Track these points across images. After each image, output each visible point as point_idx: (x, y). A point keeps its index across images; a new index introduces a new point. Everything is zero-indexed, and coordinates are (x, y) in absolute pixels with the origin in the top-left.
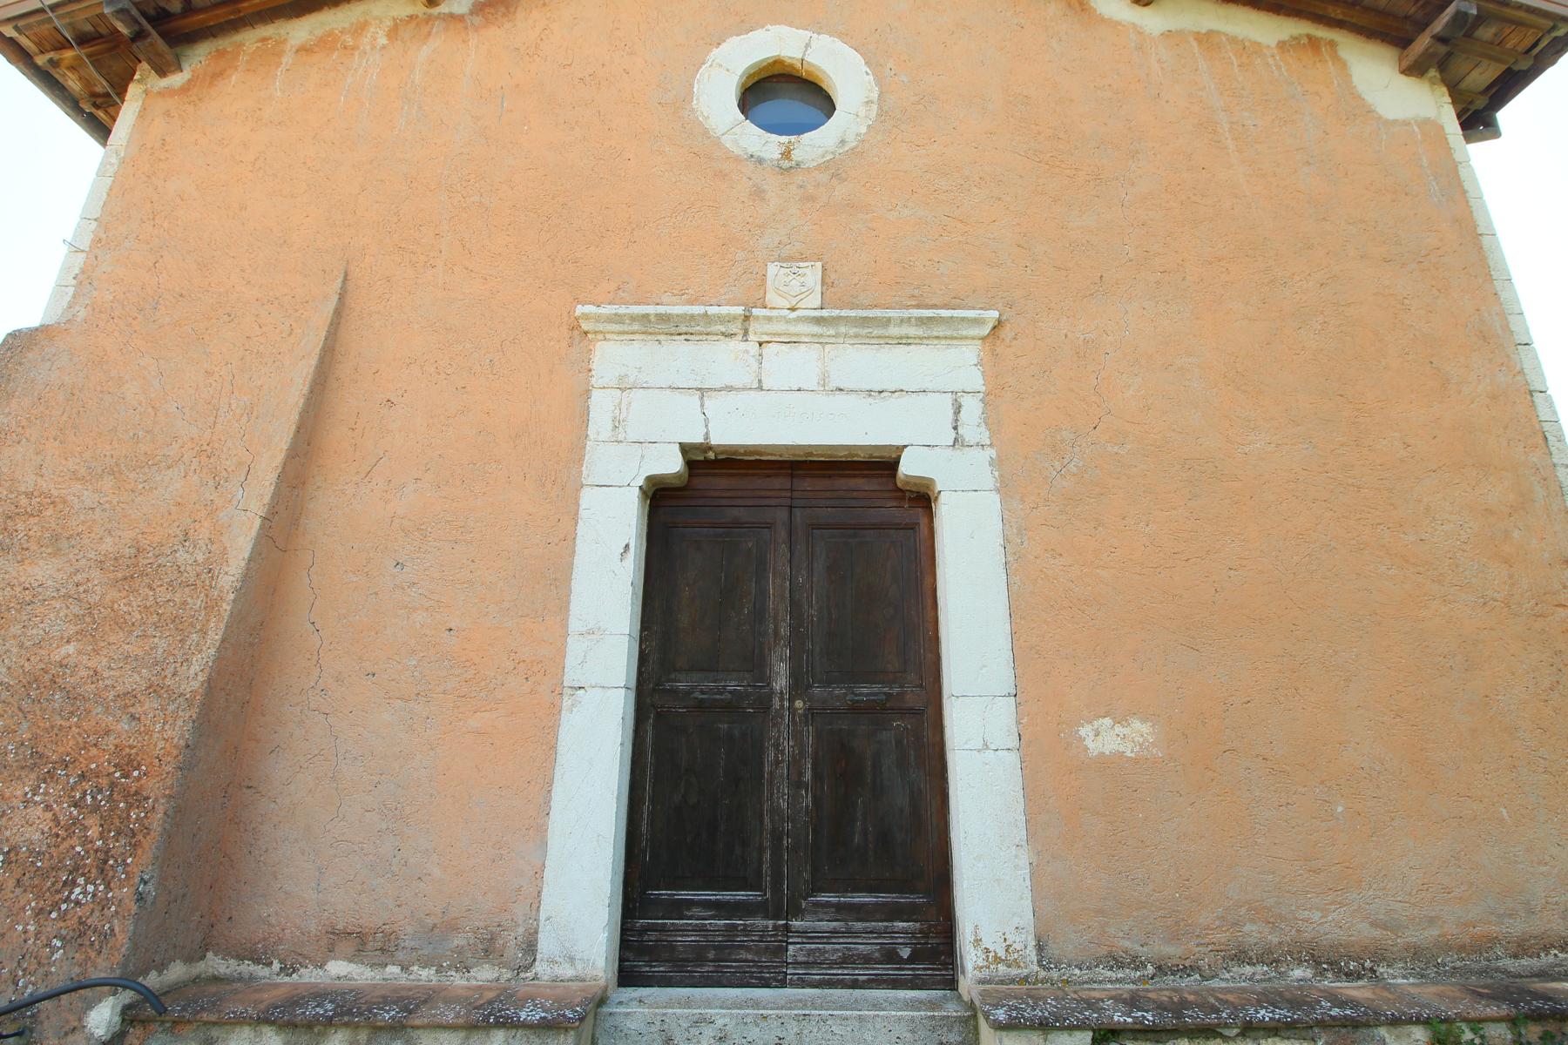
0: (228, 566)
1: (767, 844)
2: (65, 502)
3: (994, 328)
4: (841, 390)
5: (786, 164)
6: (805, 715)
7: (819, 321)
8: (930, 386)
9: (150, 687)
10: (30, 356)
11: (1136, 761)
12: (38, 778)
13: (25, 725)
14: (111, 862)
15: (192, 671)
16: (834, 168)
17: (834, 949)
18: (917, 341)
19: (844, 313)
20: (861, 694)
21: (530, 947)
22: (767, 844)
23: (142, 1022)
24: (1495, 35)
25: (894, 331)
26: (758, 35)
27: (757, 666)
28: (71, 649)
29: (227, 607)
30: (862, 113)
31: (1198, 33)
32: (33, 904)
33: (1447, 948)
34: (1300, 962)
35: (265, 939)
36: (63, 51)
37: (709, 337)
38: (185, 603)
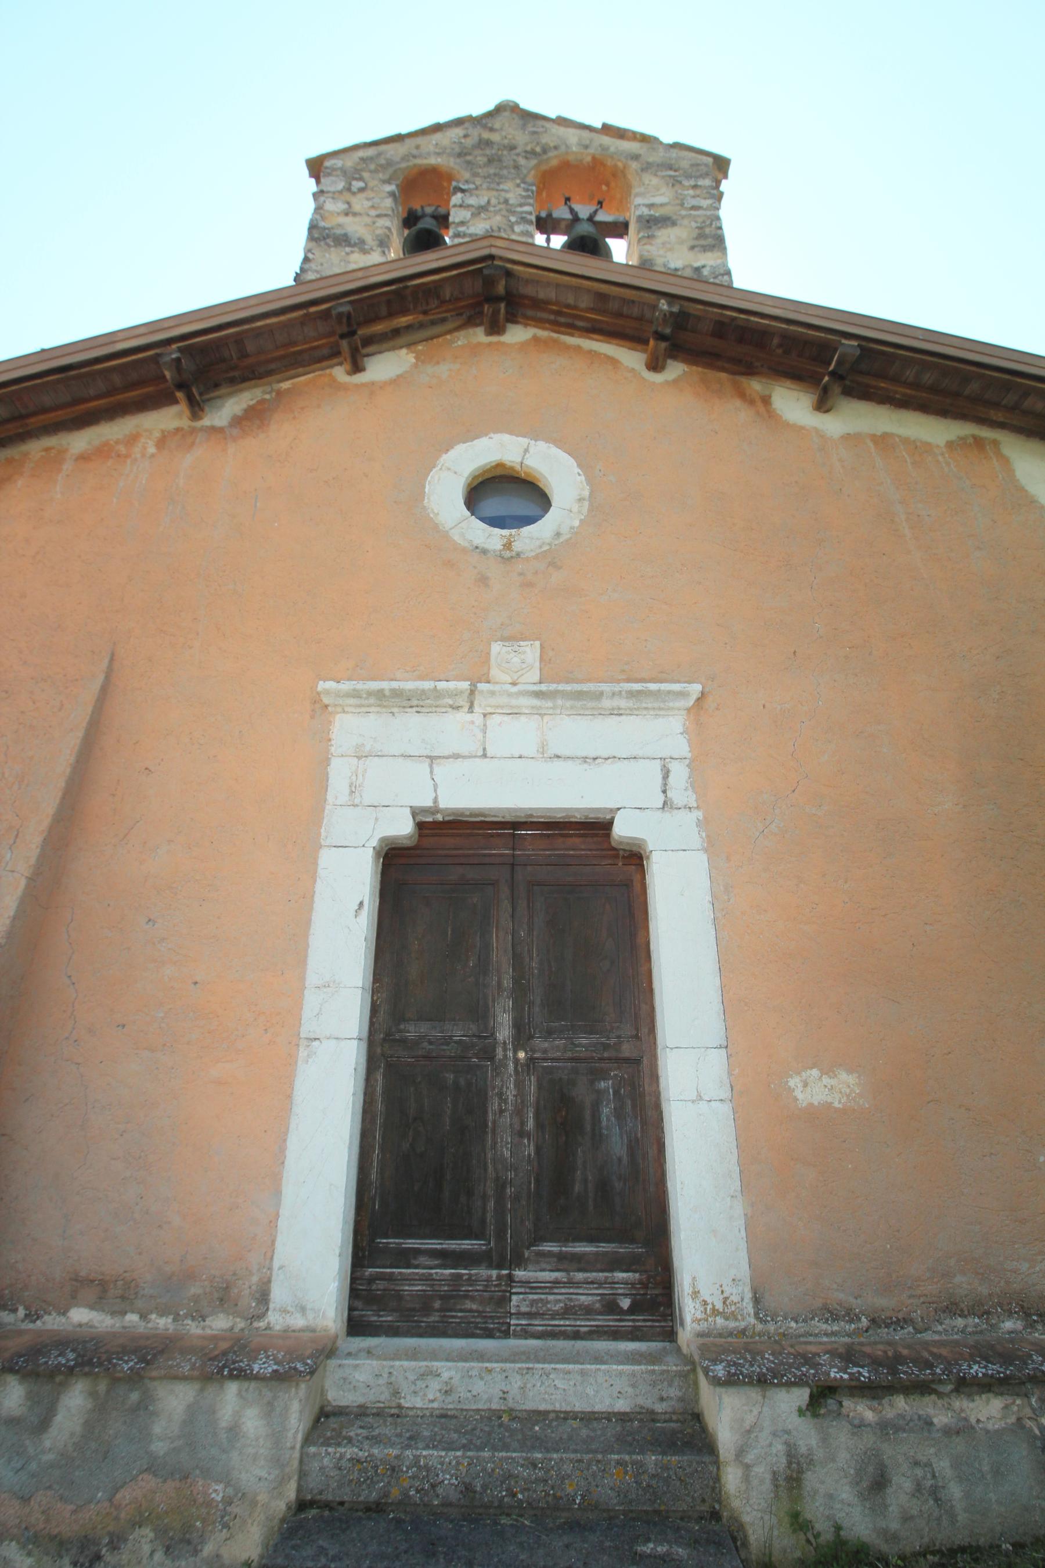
3: (698, 699)
4: (558, 757)
5: (507, 554)
6: (528, 1066)
7: (538, 695)
8: (640, 754)
17: (555, 1301)
18: (628, 712)
19: (561, 687)
21: (263, 1297)
22: (490, 1192)
26: (483, 443)
34: (1010, 1314)
37: (438, 709)
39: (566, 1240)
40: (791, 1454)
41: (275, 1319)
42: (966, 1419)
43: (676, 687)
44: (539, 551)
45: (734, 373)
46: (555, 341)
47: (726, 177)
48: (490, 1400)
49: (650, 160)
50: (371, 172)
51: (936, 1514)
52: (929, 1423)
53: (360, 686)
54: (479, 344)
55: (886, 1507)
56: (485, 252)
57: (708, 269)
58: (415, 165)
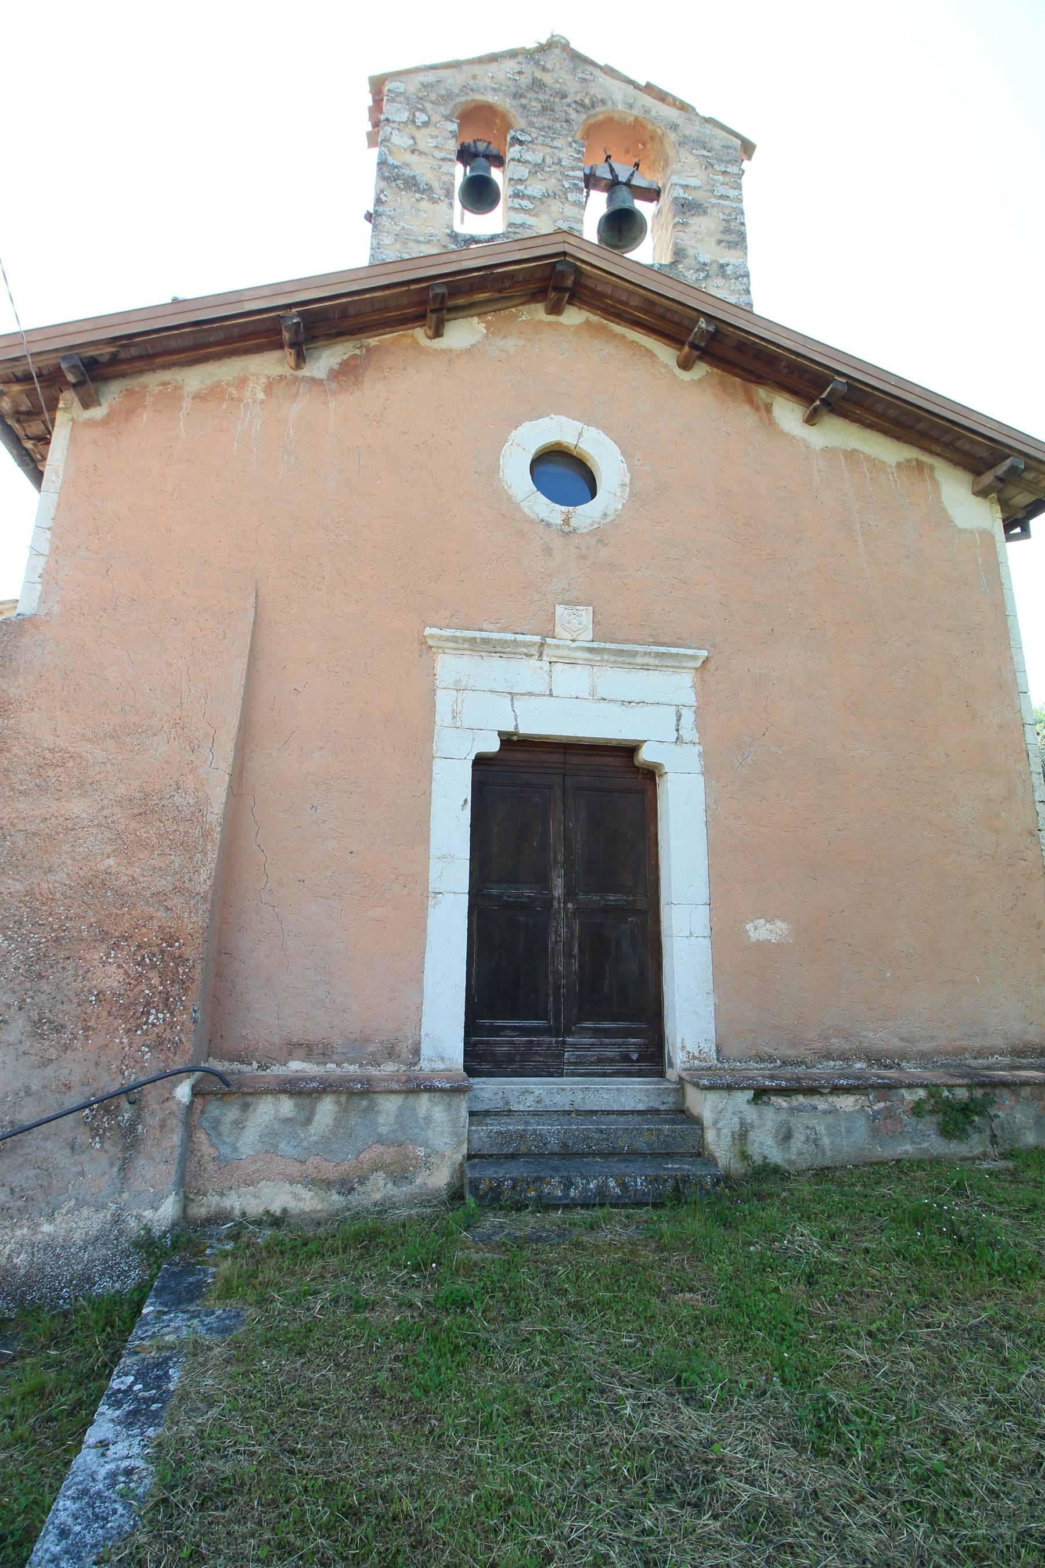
0: (212, 807)
1: (551, 992)
2: (81, 757)
3: (704, 662)
4: (604, 699)
5: (566, 529)
6: (574, 913)
7: (591, 650)
9: (175, 888)
10: (23, 641)
11: (777, 945)
12: (108, 947)
13: (91, 913)
14: (171, 999)
15: (202, 879)
16: (600, 534)
17: (592, 1054)
18: (654, 668)
19: (608, 646)
20: (609, 900)
21: (417, 1052)
22: (551, 992)
23: (203, 1094)
24: (1035, 478)
25: (639, 660)
26: (544, 422)
27: (543, 881)
28: (111, 861)
29: (217, 836)
30: (619, 494)
31: (846, 450)
32: (123, 1026)
33: (938, 1052)
34: (860, 1060)
35: (246, 1049)
36: (10, 385)
37: (516, 656)
38: (187, 832)
39: (598, 1021)
40: (742, 1123)
41: (425, 1065)
42: (835, 1106)
43: (690, 652)
44: (591, 528)
45: (746, 380)
46: (604, 328)
47: (749, 158)
48: (564, 1105)
49: (687, 133)
50: (433, 103)
51: (815, 1152)
52: (815, 1108)
53: (458, 633)
54: (540, 321)
55: (790, 1148)
56: (561, 250)
57: (730, 267)
58: (473, 100)
